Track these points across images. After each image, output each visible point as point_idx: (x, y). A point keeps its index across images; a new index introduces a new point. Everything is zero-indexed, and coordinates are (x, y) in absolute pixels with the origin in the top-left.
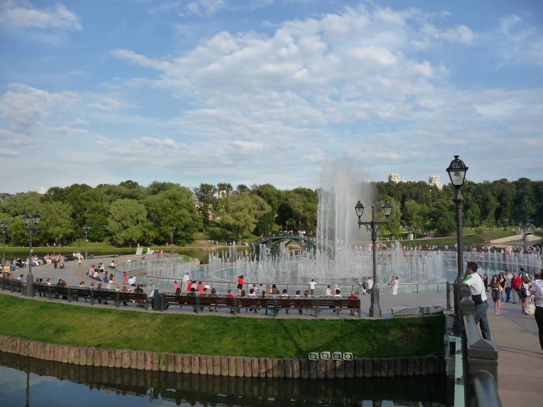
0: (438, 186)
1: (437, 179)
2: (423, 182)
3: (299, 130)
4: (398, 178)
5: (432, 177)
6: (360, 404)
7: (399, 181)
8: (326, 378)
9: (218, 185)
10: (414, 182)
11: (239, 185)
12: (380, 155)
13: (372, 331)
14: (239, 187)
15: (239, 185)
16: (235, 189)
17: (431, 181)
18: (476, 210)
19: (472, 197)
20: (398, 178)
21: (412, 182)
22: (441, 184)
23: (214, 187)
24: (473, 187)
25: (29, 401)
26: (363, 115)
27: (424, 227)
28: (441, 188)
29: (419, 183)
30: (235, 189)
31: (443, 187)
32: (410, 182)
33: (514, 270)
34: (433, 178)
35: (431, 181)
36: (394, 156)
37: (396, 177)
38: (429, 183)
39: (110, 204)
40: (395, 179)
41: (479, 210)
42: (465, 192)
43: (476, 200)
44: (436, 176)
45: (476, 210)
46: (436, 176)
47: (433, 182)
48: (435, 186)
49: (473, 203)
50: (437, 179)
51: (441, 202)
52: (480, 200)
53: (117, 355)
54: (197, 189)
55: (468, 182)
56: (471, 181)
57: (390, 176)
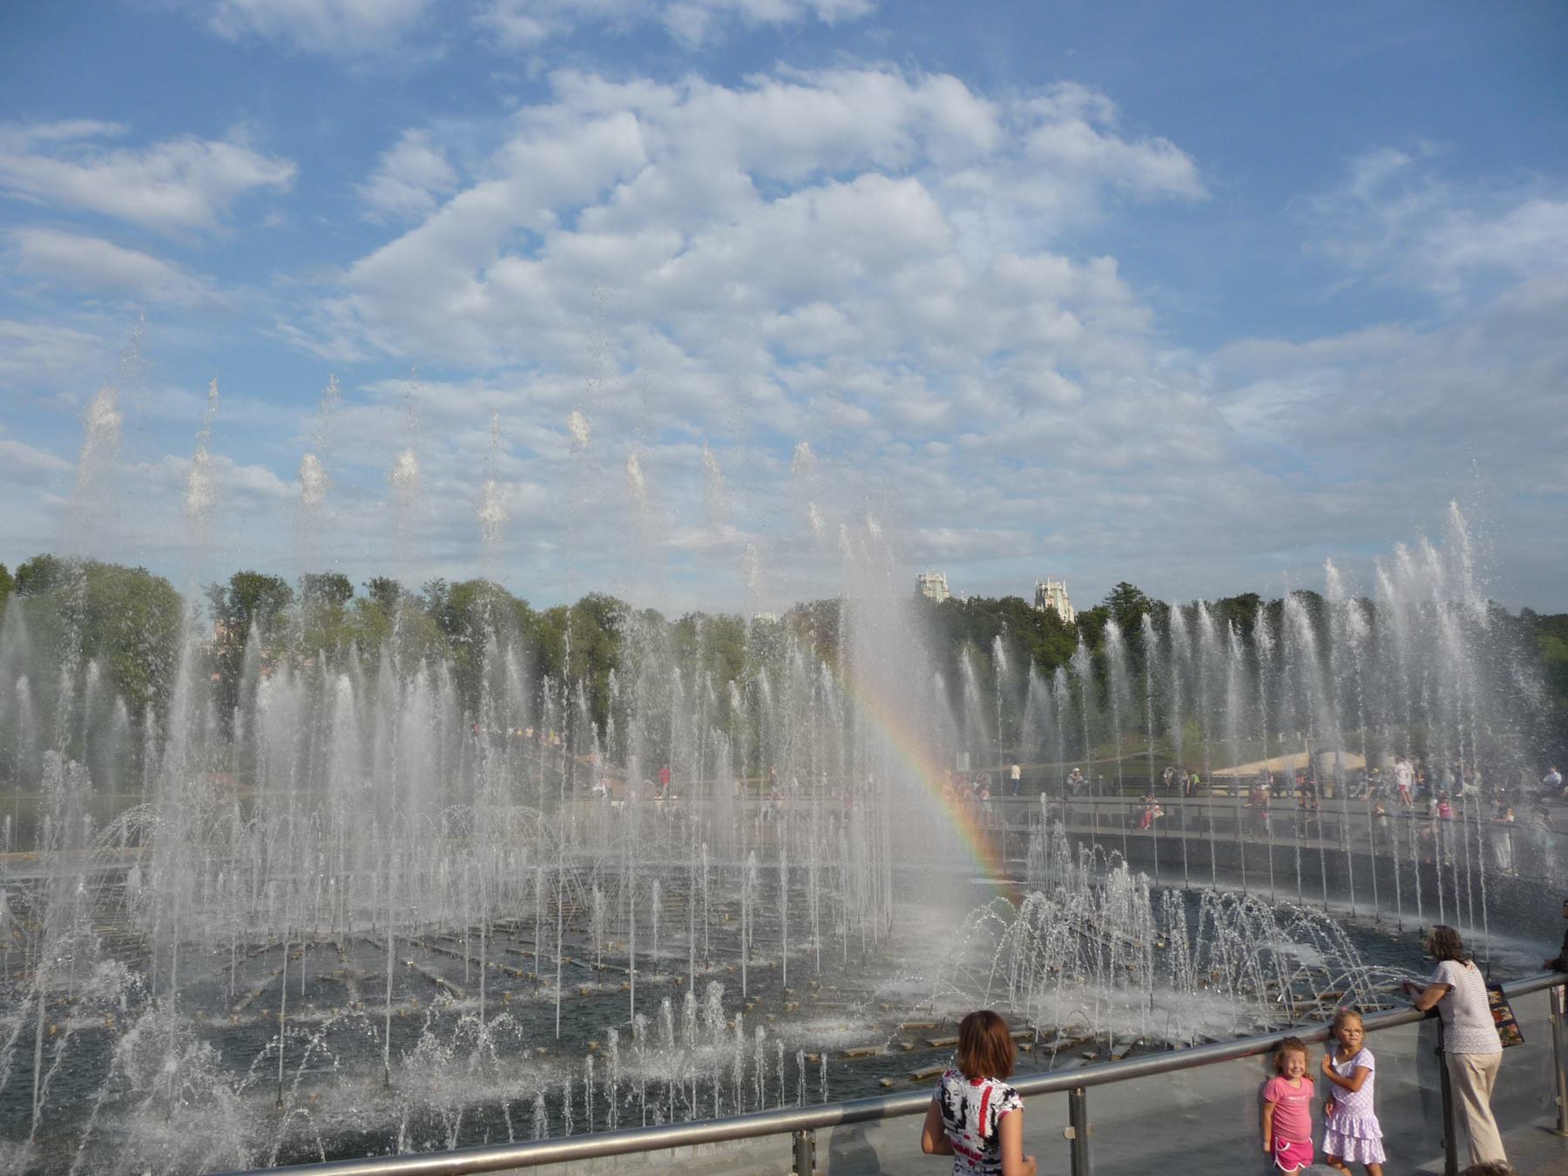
0: (1062, 615)
1: (1059, 593)
2: (1017, 599)
4: (943, 588)
5: (1043, 587)
6: (369, 1154)
7: (947, 595)
8: (339, 1152)
10: (990, 600)
13: (521, 997)
14: (1223, 602)
16: (361, 591)
17: (1040, 599)
20: (943, 588)
21: (985, 599)
23: (280, 585)
27: (40, 776)
29: (1006, 602)
30: (361, 591)
32: (979, 599)
34: (1046, 590)
35: (1040, 599)
39: (1023, 714)
44: (1057, 585)
47: (1047, 602)
48: (1052, 612)
50: (1059, 593)
51: (1058, 649)
53: (1524, 960)
54: (223, 590)
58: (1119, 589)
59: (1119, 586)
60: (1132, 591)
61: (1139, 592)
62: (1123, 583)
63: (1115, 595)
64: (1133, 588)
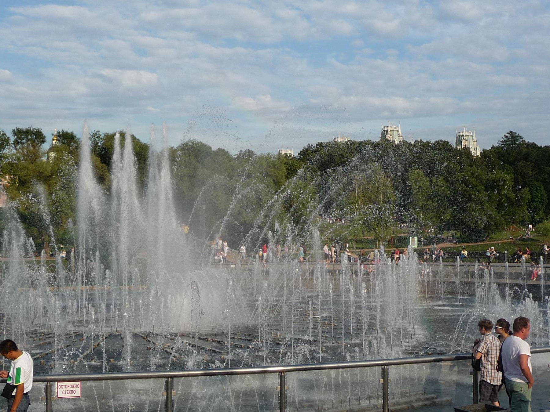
1: (471, 138)
3: (228, 51)
7: (401, 139)
9: (14, 131)
10: (428, 142)
11: (59, 133)
12: (376, 101)
14: (59, 136)
15: (59, 133)
17: (459, 142)
18: (539, 196)
19: (532, 171)
22: (478, 148)
24: (536, 152)
25: (268, 374)
26: (346, 28)
28: (479, 154)
31: (481, 153)
33: (354, 241)
35: (459, 142)
36: (400, 103)
37: (396, 133)
38: (457, 145)
40: (392, 135)
41: (546, 195)
42: (519, 161)
43: (540, 177)
45: (539, 196)
46: (469, 133)
47: (463, 143)
48: (467, 150)
49: (535, 181)
50: (471, 138)
51: (472, 174)
52: (546, 176)
55: (526, 144)
56: (531, 142)
57: (384, 131)
58: (509, 135)
59: (508, 133)
60: (517, 137)
61: (521, 137)
62: (511, 132)
63: (506, 139)
64: (517, 135)
